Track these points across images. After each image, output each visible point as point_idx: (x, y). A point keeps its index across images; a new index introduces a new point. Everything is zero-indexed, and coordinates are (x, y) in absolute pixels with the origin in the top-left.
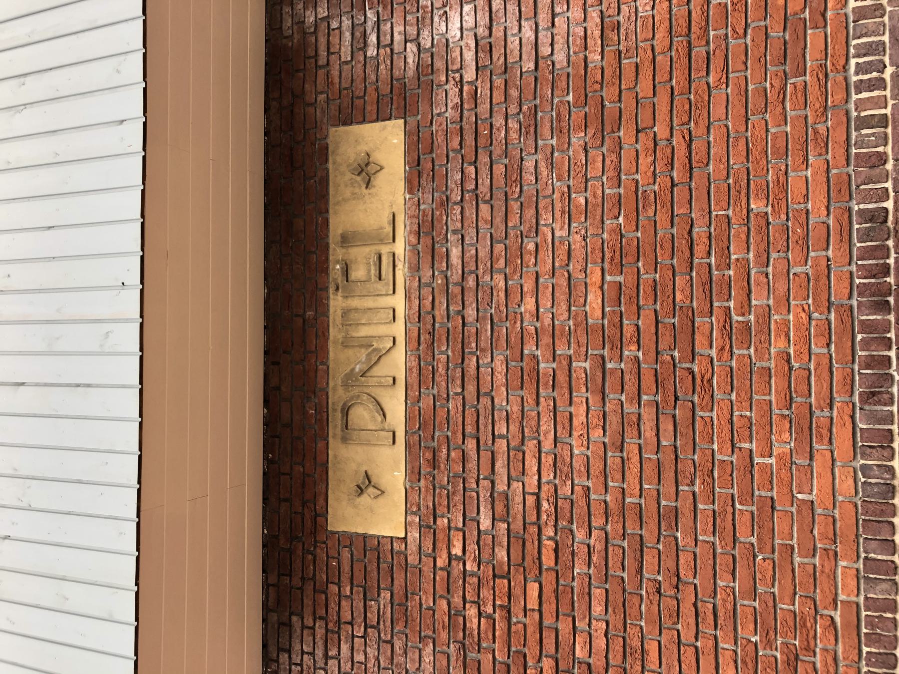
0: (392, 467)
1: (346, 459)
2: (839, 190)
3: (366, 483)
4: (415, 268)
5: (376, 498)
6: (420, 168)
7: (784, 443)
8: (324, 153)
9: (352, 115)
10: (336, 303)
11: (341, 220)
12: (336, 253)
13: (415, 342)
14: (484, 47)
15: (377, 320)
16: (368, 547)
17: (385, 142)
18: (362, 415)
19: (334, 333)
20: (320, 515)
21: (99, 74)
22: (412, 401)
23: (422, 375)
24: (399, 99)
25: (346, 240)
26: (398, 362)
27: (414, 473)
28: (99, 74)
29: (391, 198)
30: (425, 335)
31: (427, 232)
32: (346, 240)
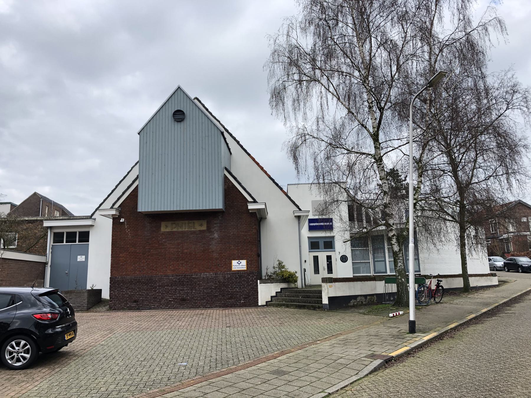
0: (168, 230)
1: (169, 223)
2: (195, 272)
3: (167, 226)
4: (190, 231)
5: (165, 228)
6: (203, 231)
7: (173, 269)
8: (203, 220)
9: (208, 223)
10: (187, 222)
11: (196, 222)
12: (192, 221)
13: (182, 231)
14: (213, 238)
15: (185, 227)
16: (160, 227)
17: (204, 228)
18: (174, 225)
19: (183, 222)
20: (163, 221)
21: (198, 205)
22: (176, 232)
23: (178, 232)
24: (209, 228)
25: (194, 223)
26: (180, 230)
27: (168, 232)
28: (198, 205)
29: (519, 95)
30: (183, 233)
31: (194, 232)
32: (194, 223)
